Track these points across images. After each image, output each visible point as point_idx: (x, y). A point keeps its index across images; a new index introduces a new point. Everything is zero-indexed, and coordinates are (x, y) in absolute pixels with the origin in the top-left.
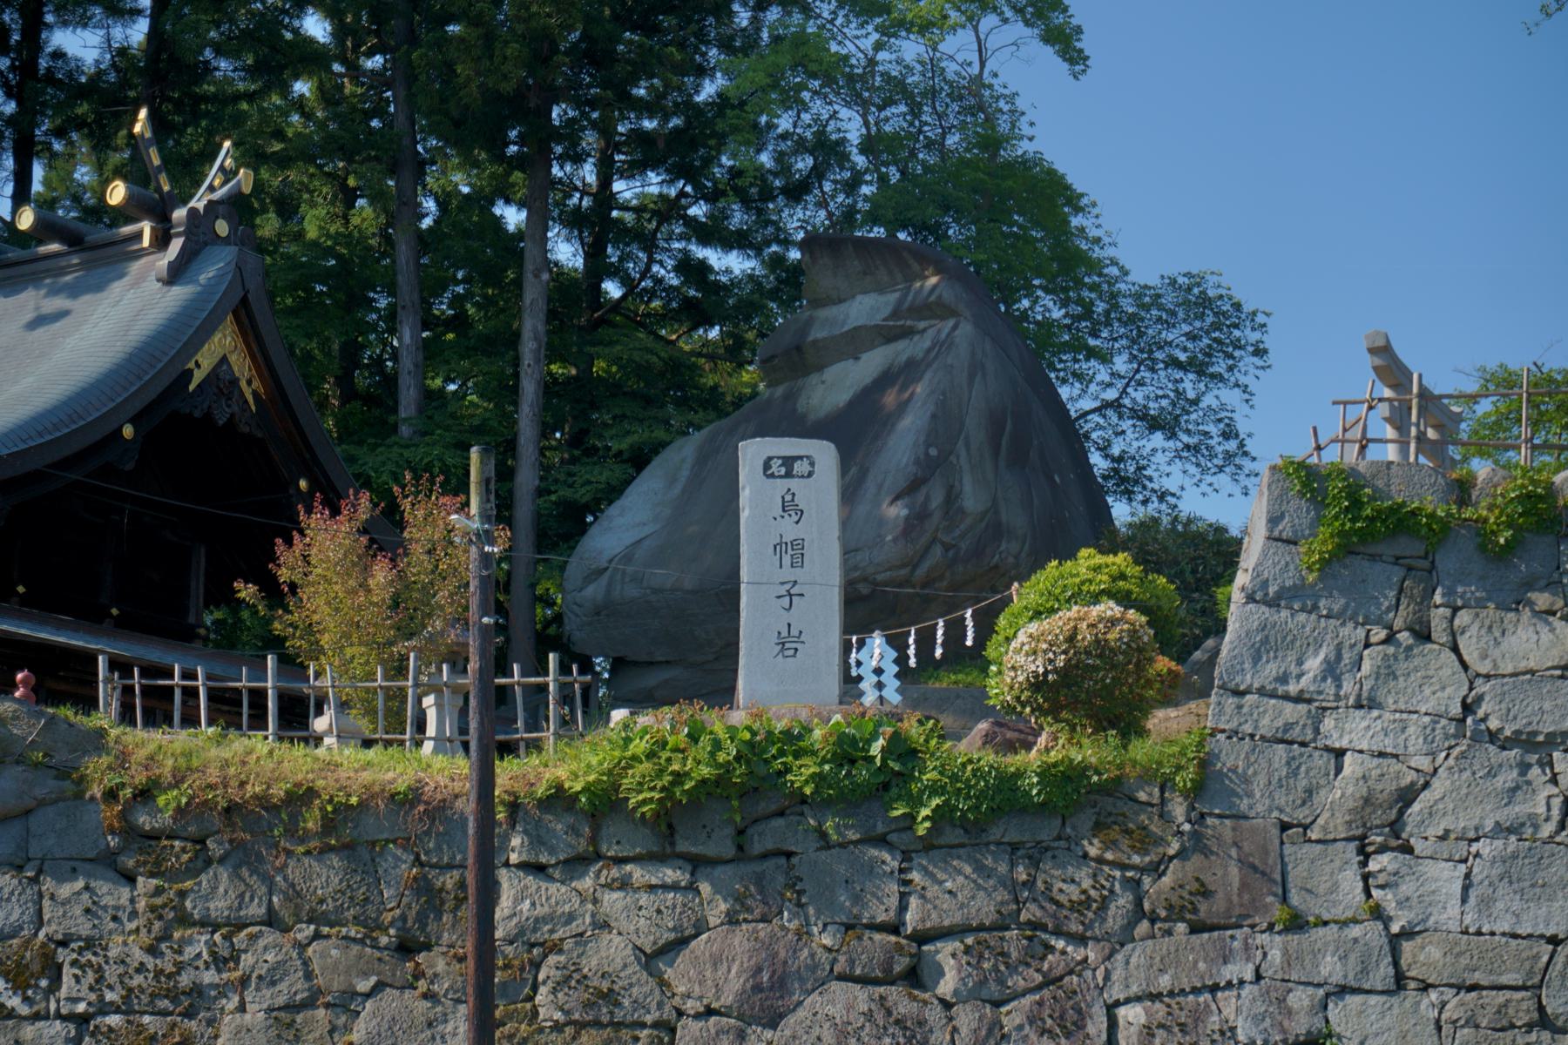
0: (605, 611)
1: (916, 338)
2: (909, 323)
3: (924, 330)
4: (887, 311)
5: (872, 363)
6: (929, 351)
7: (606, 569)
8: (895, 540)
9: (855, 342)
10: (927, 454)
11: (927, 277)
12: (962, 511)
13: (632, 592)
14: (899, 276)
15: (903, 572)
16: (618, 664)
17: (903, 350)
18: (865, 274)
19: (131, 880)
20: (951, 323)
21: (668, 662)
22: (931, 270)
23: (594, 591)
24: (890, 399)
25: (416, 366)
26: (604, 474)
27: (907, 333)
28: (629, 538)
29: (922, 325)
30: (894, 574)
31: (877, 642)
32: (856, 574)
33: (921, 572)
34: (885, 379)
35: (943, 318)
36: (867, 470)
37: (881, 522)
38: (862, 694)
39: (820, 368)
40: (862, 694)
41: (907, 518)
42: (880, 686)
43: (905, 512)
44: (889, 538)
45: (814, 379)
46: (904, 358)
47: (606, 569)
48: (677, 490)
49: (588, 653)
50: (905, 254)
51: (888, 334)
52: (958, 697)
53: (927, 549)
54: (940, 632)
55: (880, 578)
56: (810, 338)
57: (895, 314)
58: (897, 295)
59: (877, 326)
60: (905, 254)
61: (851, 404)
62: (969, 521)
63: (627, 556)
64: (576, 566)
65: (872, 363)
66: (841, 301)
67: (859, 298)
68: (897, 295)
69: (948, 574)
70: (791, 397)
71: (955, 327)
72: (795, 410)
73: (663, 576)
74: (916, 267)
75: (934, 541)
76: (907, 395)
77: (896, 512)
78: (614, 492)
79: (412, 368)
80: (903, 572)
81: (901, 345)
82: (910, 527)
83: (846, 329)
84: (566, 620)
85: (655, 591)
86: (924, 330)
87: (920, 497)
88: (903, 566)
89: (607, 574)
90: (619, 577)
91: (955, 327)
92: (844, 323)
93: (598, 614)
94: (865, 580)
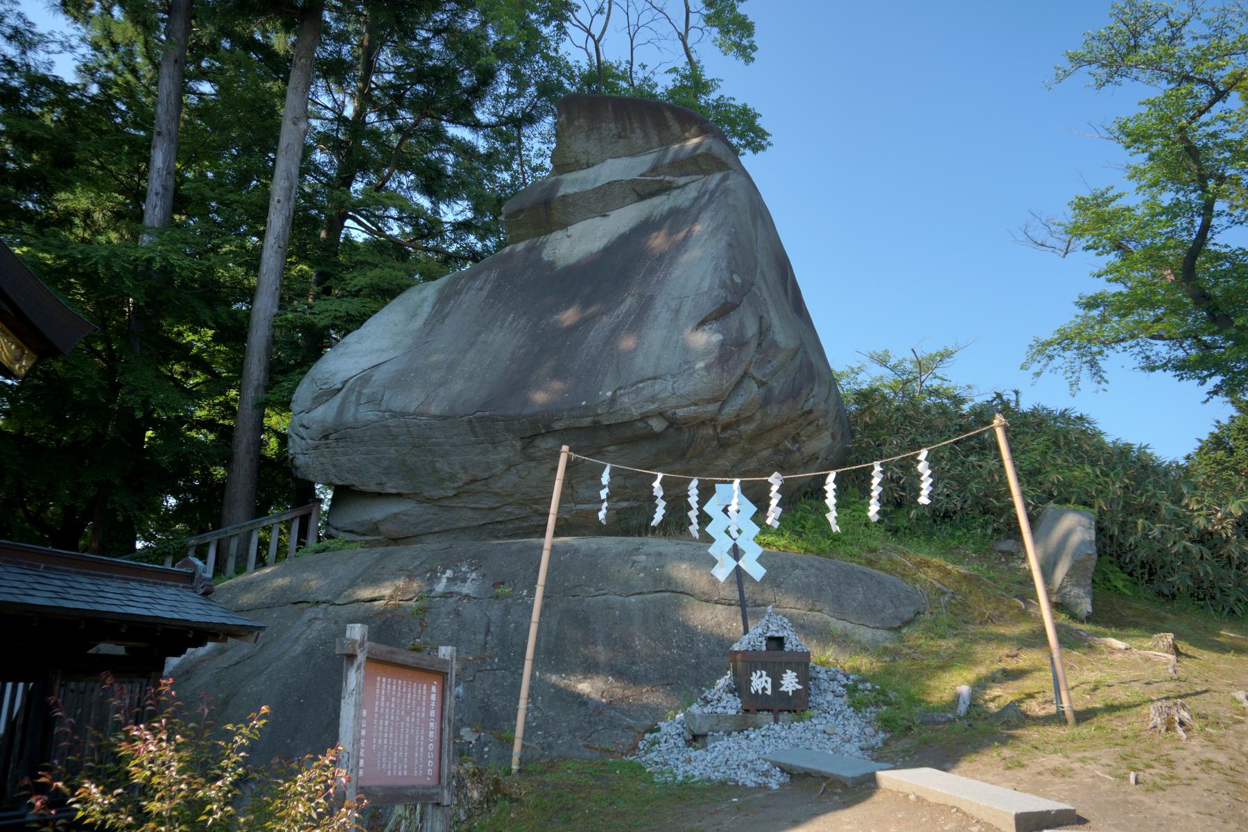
0: (330, 435)
1: (675, 193)
2: (668, 178)
3: (685, 185)
4: (645, 168)
5: (624, 218)
6: (696, 199)
7: (339, 390)
8: (708, 368)
9: (603, 200)
10: (732, 280)
11: (687, 139)
12: (774, 344)
13: (367, 414)
14: (655, 139)
15: (712, 408)
16: (343, 494)
17: (659, 205)
18: (620, 137)
19: (720, 314)
20: (718, 176)
21: (399, 495)
22: (694, 130)
23: (325, 413)
24: (658, 241)
25: (165, 188)
26: (337, 306)
27: (664, 189)
28: (366, 362)
29: (682, 180)
30: (700, 409)
31: (731, 493)
32: (652, 407)
33: (730, 411)
34: (645, 227)
35: (706, 173)
36: (652, 297)
37: (686, 350)
38: (713, 562)
39: (564, 226)
40: (713, 562)
41: (722, 344)
42: (736, 553)
43: (717, 338)
44: (701, 365)
45: (559, 234)
46: (666, 208)
47: (339, 390)
48: (419, 322)
49: (311, 478)
50: (668, 114)
51: (642, 191)
52: (794, 566)
53: (738, 384)
54: (876, 481)
55: (680, 413)
56: (560, 193)
57: (654, 169)
58: (654, 155)
59: (633, 181)
60: (668, 114)
61: (607, 250)
62: (781, 357)
63: (365, 378)
64: (304, 392)
65: (624, 218)
66: (589, 166)
67: (610, 161)
68: (654, 155)
69: (758, 416)
70: (534, 250)
71: (725, 179)
72: (541, 259)
73: (409, 401)
74: (675, 127)
75: (745, 374)
76: (682, 235)
77: (704, 339)
78: (353, 322)
79: (160, 190)
80: (712, 408)
81: (656, 200)
82: (725, 355)
83: (599, 184)
84: (290, 443)
85: (395, 414)
86: (685, 185)
87: (733, 321)
88: (715, 400)
89: (341, 394)
90: (353, 398)
91: (725, 179)
92: (596, 180)
93: (326, 437)
94: (661, 414)
